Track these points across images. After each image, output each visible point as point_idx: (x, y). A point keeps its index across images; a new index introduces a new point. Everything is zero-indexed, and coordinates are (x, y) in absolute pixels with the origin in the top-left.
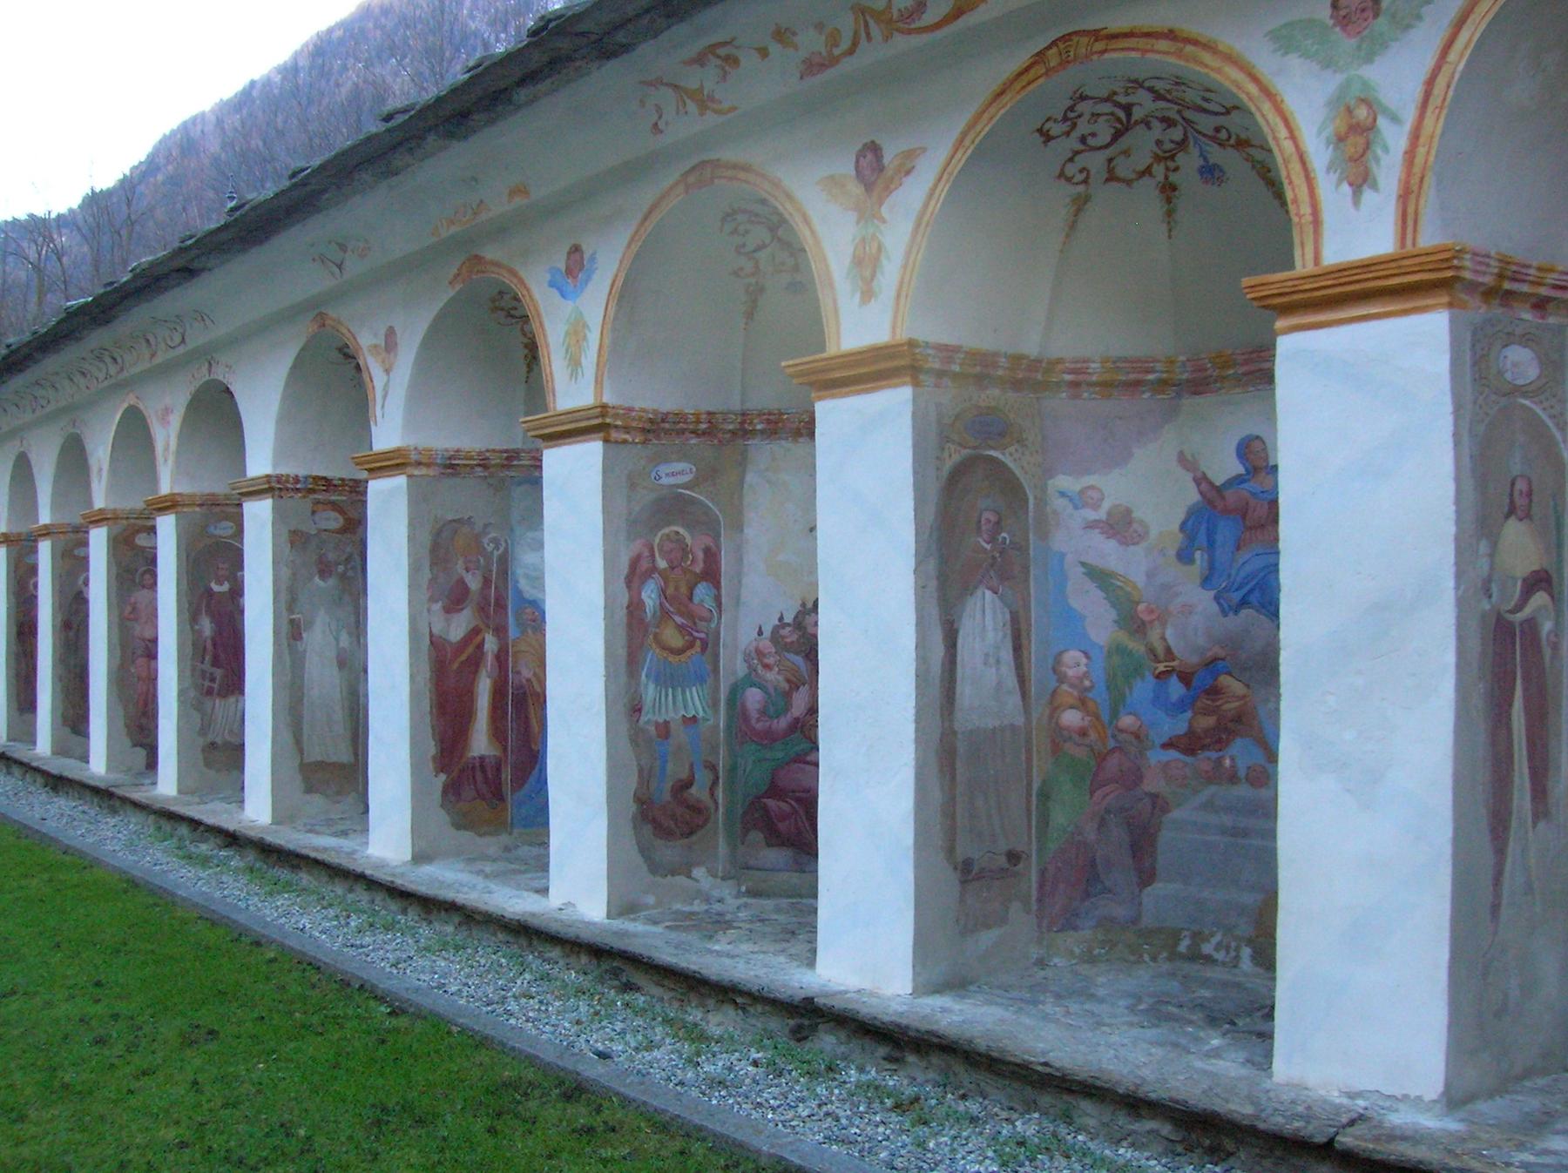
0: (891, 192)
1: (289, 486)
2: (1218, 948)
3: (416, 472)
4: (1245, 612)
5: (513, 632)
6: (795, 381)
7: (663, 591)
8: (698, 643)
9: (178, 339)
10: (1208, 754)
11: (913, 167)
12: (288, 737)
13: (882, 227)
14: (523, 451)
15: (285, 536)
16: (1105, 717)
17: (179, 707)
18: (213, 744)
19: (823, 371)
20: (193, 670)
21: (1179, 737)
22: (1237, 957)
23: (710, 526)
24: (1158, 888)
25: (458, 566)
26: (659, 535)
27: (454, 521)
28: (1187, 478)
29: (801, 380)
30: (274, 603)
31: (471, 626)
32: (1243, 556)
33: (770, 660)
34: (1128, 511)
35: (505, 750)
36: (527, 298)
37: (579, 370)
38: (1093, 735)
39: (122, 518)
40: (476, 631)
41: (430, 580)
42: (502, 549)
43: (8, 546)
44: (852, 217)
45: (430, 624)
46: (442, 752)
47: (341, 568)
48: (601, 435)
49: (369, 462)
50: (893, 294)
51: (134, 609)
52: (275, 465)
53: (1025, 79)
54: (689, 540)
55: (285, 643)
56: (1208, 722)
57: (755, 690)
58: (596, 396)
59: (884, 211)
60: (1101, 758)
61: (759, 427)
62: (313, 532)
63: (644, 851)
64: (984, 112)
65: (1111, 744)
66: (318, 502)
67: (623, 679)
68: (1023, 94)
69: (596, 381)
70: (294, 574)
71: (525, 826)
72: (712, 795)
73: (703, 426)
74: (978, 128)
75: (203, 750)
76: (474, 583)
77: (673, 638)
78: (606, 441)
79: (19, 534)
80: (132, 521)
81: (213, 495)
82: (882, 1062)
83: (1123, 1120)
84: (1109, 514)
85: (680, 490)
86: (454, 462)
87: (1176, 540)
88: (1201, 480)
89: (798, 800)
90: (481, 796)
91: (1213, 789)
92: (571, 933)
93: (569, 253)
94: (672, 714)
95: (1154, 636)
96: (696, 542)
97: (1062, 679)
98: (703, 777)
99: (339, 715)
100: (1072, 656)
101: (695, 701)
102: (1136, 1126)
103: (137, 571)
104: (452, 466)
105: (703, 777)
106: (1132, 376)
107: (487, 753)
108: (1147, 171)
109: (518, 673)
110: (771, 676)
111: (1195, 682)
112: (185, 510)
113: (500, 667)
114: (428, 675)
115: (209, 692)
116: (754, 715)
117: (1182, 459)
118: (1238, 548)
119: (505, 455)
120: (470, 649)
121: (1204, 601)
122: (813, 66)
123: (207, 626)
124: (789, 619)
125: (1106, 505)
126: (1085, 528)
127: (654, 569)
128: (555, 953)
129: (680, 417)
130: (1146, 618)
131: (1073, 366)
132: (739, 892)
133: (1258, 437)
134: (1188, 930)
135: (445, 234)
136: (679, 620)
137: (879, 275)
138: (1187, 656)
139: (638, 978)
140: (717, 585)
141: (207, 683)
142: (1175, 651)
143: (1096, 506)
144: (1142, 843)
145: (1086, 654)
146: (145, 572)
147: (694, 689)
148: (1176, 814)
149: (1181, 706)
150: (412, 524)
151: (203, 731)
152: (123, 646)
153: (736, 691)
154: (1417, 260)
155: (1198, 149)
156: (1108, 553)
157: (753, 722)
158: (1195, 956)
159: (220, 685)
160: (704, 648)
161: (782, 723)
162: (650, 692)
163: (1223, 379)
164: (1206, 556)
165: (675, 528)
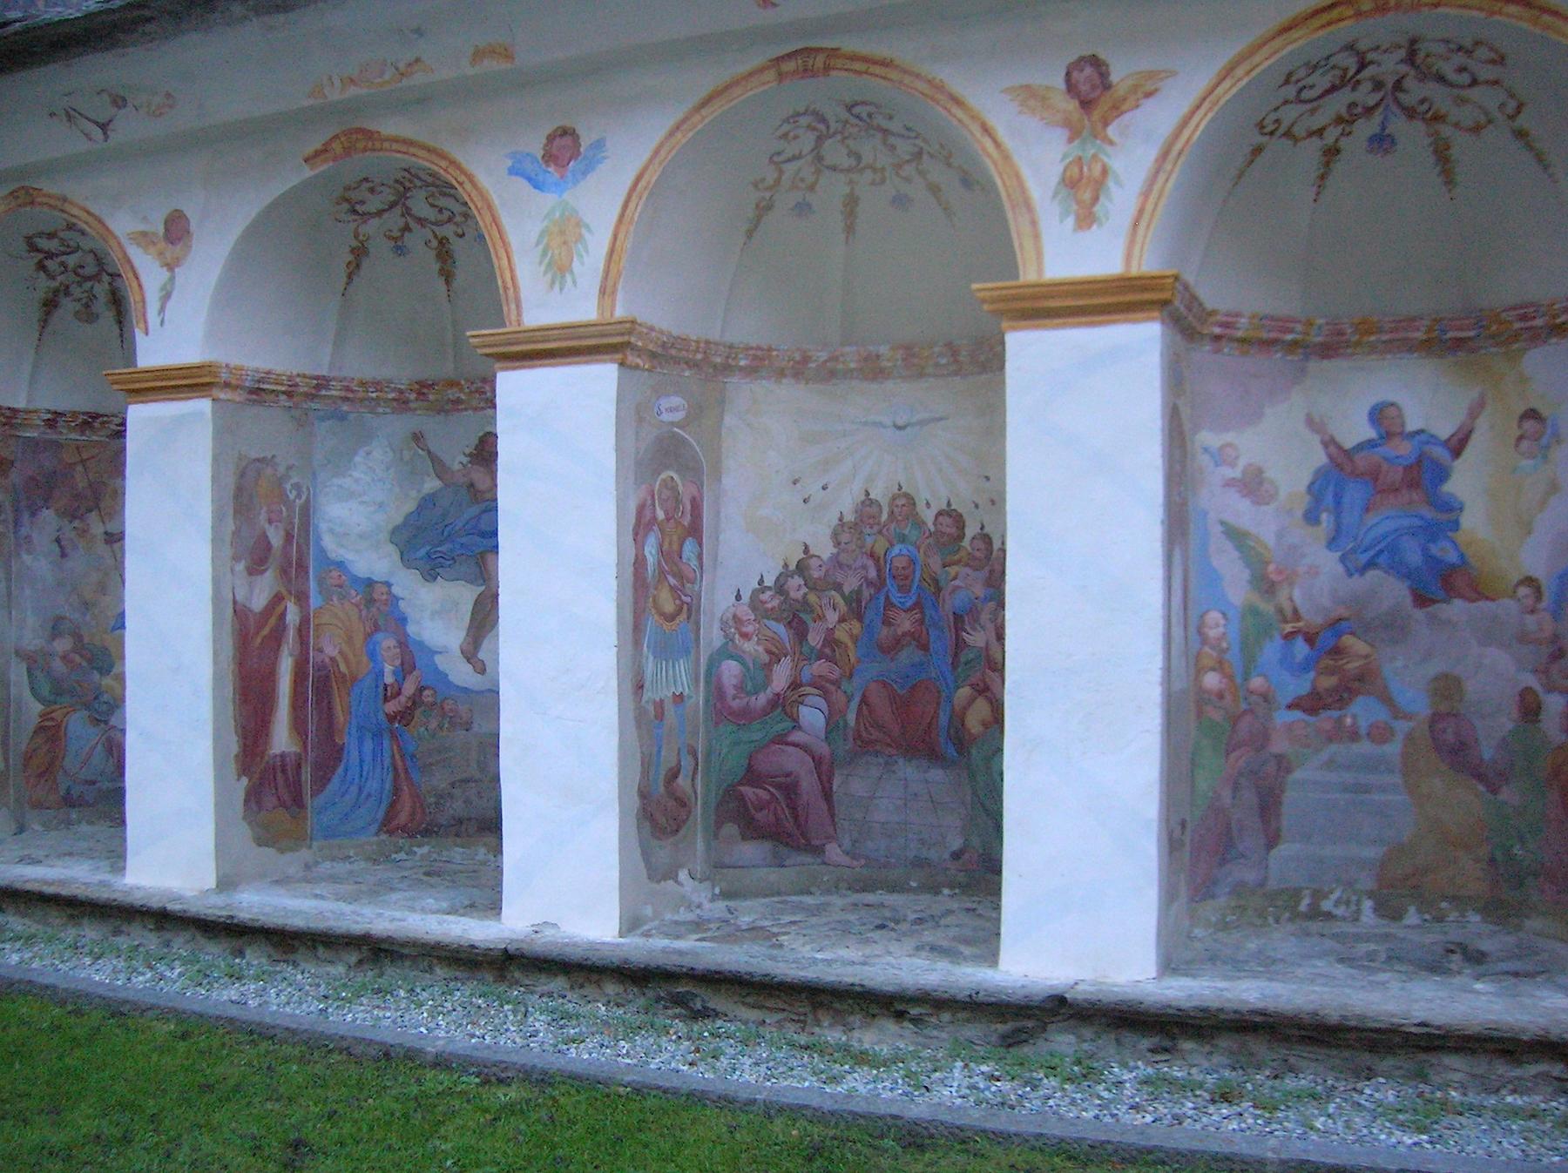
0: (1122, 113)
2: (1337, 903)
3: (222, 396)
4: (1373, 575)
5: (315, 600)
6: (986, 307)
7: (661, 546)
8: (685, 607)
10: (1329, 713)
11: (1156, 90)
13: (1108, 149)
14: (334, 379)
16: (1239, 680)
21: (1300, 698)
22: (1358, 911)
23: (693, 470)
24: (1284, 849)
25: (261, 518)
26: (659, 479)
27: (258, 460)
28: (1315, 440)
29: (992, 307)
31: (274, 592)
32: (1372, 519)
33: (749, 629)
34: (1260, 471)
35: (305, 746)
36: (468, 186)
37: (569, 278)
38: (1228, 697)
40: (278, 599)
41: (234, 533)
42: (304, 498)
44: (1060, 135)
45: (234, 588)
46: (244, 751)
48: (619, 356)
49: (124, 383)
50: (1127, 221)
53: (1325, 17)
54: (681, 489)
56: (1328, 682)
57: (734, 663)
58: (601, 306)
59: (1111, 131)
60: (1235, 720)
61: (742, 363)
64: (1264, 44)
65: (1243, 706)
67: (629, 647)
68: (1321, 33)
69: (603, 291)
71: (326, 838)
72: (693, 785)
74: (1257, 59)
76: (276, 538)
78: (622, 364)
82: (1149, 1055)
83: (1502, 1069)
84: (1244, 472)
85: (676, 429)
86: (262, 386)
87: (1305, 502)
88: (1329, 443)
89: (779, 786)
90: (282, 804)
91: (1334, 748)
92: (576, 954)
93: (551, 138)
94: (666, 693)
95: (1282, 596)
96: (685, 490)
97: (1204, 640)
98: (687, 762)
100: (1214, 616)
102: (1517, 1072)
104: (259, 391)
105: (687, 762)
106: (1273, 335)
107: (287, 750)
108: (1320, 132)
109: (321, 650)
110: (749, 647)
111: (1318, 643)
113: (301, 644)
114: (231, 654)
116: (731, 692)
117: (1310, 421)
118: (1367, 510)
119: (315, 382)
120: (273, 621)
121: (1328, 563)
124: (769, 582)
125: (1242, 463)
126: (1224, 486)
128: (559, 983)
130: (1273, 577)
131: (1224, 319)
132: (714, 895)
133: (1392, 404)
134: (1307, 888)
135: (334, 95)
136: (672, 581)
137: (1102, 199)
138: (1312, 619)
139: (717, 1002)
142: (1302, 611)
143: (1233, 465)
144: (1269, 806)
145: (1224, 614)
147: (681, 661)
148: (1298, 775)
149: (1305, 667)
150: (216, 459)
153: (714, 662)
154: (510, 284)
155: (1382, 117)
156: (1241, 511)
157: (729, 698)
158: (1315, 914)
161: (762, 700)
162: (650, 666)
163: (1358, 344)
164: (1332, 518)
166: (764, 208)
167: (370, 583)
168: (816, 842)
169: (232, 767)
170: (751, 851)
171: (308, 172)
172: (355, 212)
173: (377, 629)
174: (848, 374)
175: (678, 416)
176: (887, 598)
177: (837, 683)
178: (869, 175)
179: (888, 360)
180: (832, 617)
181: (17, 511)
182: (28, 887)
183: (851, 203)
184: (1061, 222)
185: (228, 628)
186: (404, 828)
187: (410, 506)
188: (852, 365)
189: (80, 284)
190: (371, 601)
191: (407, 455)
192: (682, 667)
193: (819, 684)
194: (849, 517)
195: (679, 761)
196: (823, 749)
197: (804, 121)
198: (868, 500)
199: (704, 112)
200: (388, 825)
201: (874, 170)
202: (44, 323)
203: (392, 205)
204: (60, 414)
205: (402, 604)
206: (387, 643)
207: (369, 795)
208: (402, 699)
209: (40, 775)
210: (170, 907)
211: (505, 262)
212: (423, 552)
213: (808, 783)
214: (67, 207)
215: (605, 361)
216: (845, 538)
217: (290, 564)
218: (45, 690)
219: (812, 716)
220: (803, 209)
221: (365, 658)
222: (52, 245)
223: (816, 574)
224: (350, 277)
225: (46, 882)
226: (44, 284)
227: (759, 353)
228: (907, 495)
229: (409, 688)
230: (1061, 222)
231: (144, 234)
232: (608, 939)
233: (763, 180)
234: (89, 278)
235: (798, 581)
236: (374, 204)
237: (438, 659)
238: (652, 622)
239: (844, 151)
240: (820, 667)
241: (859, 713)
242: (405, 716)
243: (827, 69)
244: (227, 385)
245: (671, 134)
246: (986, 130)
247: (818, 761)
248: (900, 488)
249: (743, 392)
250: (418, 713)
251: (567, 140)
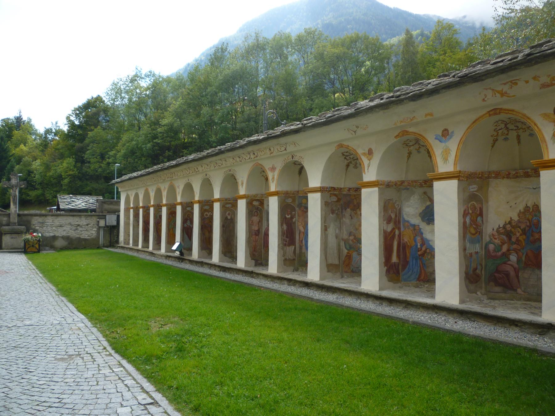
3: (380, 187)
5: (402, 229)
8: (478, 232)
9: (283, 149)
12: (324, 257)
14: (406, 181)
15: (324, 203)
17: (278, 249)
18: (286, 259)
19: (545, 163)
20: (282, 239)
27: (389, 200)
33: (496, 237)
35: (400, 260)
36: (427, 142)
37: (448, 162)
40: (393, 229)
47: (337, 212)
48: (458, 178)
51: (252, 222)
52: (321, 184)
54: (476, 206)
55: (323, 232)
57: (492, 245)
61: (493, 176)
63: (467, 286)
66: (331, 194)
69: (454, 164)
70: (326, 213)
73: (480, 176)
75: (284, 261)
76: (393, 216)
77: (473, 231)
78: (459, 180)
79: (202, 201)
80: (252, 198)
93: (443, 131)
94: (473, 251)
96: (477, 206)
98: (479, 267)
99: (336, 251)
101: (477, 247)
104: (388, 185)
105: (479, 267)
109: (404, 240)
115: (285, 245)
116: (492, 251)
120: (392, 234)
122: (544, 86)
123: (285, 227)
124: (501, 226)
127: (469, 213)
129: (476, 173)
135: (398, 125)
136: (474, 226)
140: (482, 217)
141: (285, 242)
146: (255, 212)
151: (284, 256)
153: (487, 245)
154: (436, 163)
157: (491, 253)
159: (288, 243)
160: (479, 234)
161: (500, 253)
162: (468, 245)
165: (473, 202)
166: (495, 141)
167: (414, 226)
168: (515, 288)
169: (383, 265)
170: (498, 289)
171: (395, 140)
172: (407, 146)
173: (416, 235)
174: (521, 177)
175: (475, 189)
176: (532, 230)
177: (519, 250)
178: (521, 130)
179: (531, 173)
180: (518, 234)
181: (342, 210)
182: (342, 288)
183: (518, 137)
184: (553, 145)
185: (382, 235)
186: (422, 280)
187: (424, 208)
188: (522, 174)
189: (354, 161)
190: (415, 229)
191: (423, 197)
192: (477, 246)
193: (516, 251)
194: (522, 211)
195: (477, 267)
196: (516, 266)
197: (500, 122)
198: (527, 206)
199: (474, 124)
200: (419, 279)
201: (523, 129)
202: (347, 169)
203: (415, 144)
204: (351, 189)
205: (422, 230)
206: (418, 239)
207: (414, 272)
208: (422, 251)
209: (346, 266)
210: (369, 293)
211: (435, 158)
212: (426, 219)
213: (512, 273)
214: (349, 148)
215: (455, 179)
216: (521, 215)
217: (396, 222)
218: (348, 247)
219: (513, 258)
220: (506, 139)
221: (413, 242)
222: (347, 154)
223: (514, 224)
224: (408, 159)
225: (345, 287)
226: (346, 162)
227: (497, 173)
228: (536, 205)
229: (424, 249)
230: (553, 145)
231: (364, 153)
232: (456, 304)
233: (494, 135)
234: (355, 160)
235: (509, 226)
236: (411, 144)
237: (430, 242)
238: (468, 236)
239: (514, 126)
240: (515, 246)
241: (526, 257)
242: (423, 255)
243: (500, 113)
244: (381, 184)
245: (467, 129)
246: (535, 124)
247: (515, 269)
248: (535, 203)
249: (494, 183)
250: (426, 254)
251: (446, 132)
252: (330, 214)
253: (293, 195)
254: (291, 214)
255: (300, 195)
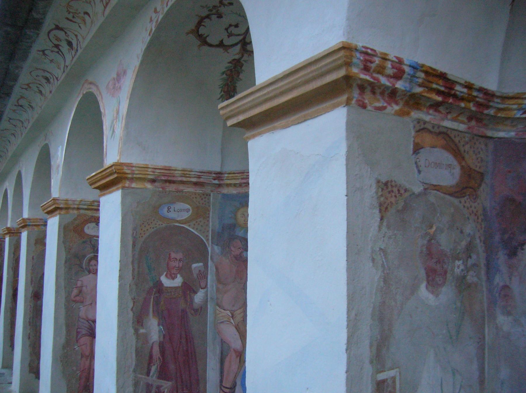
1: (384, 80)
30: (348, 349)
39: (74, 208)
43: (9, 236)
51: (80, 291)
62: (418, 189)
70: (386, 280)
80: (82, 212)
81: (169, 169)
103: (84, 256)
112: (134, 185)
152: (69, 326)
181: (490, 251)
252: (414, 289)
253: (199, 190)
254: (185, 270)
255: (225, 191)
